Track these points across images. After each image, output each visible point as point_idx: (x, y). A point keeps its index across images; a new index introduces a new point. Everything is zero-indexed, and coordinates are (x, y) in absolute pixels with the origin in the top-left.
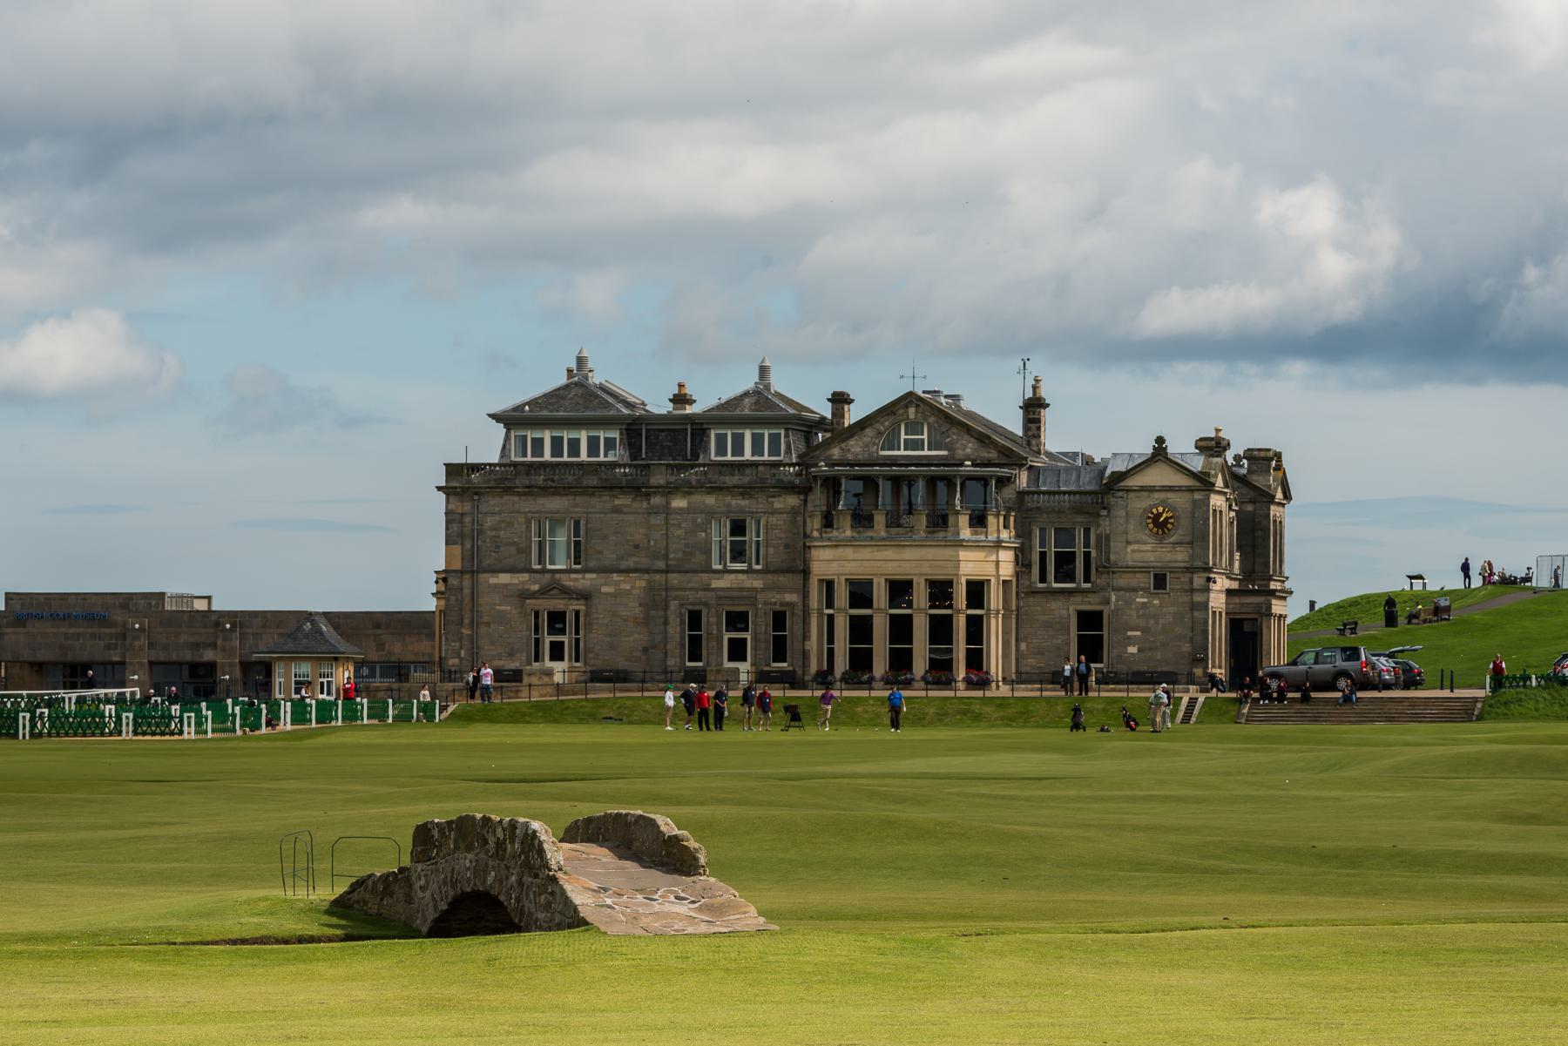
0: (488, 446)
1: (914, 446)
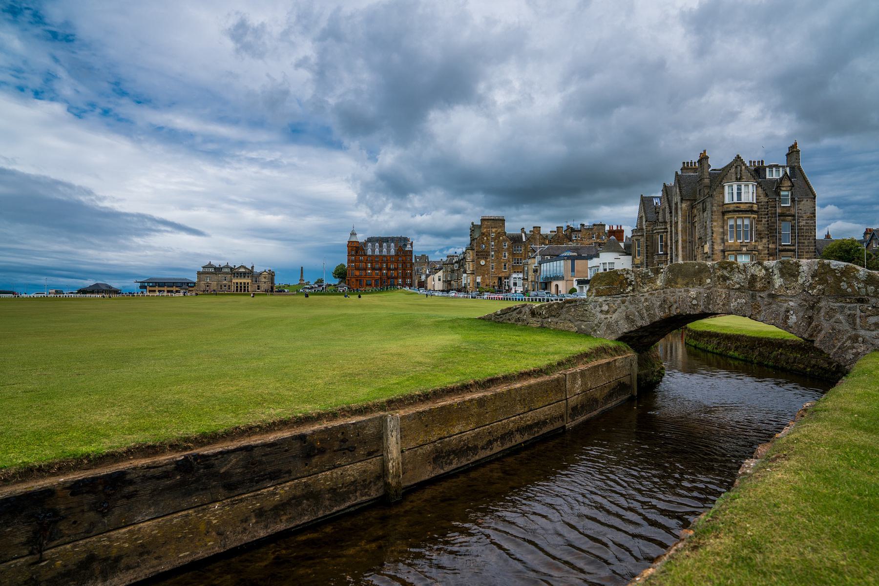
0: (201, 270)
1: (242, 270)
